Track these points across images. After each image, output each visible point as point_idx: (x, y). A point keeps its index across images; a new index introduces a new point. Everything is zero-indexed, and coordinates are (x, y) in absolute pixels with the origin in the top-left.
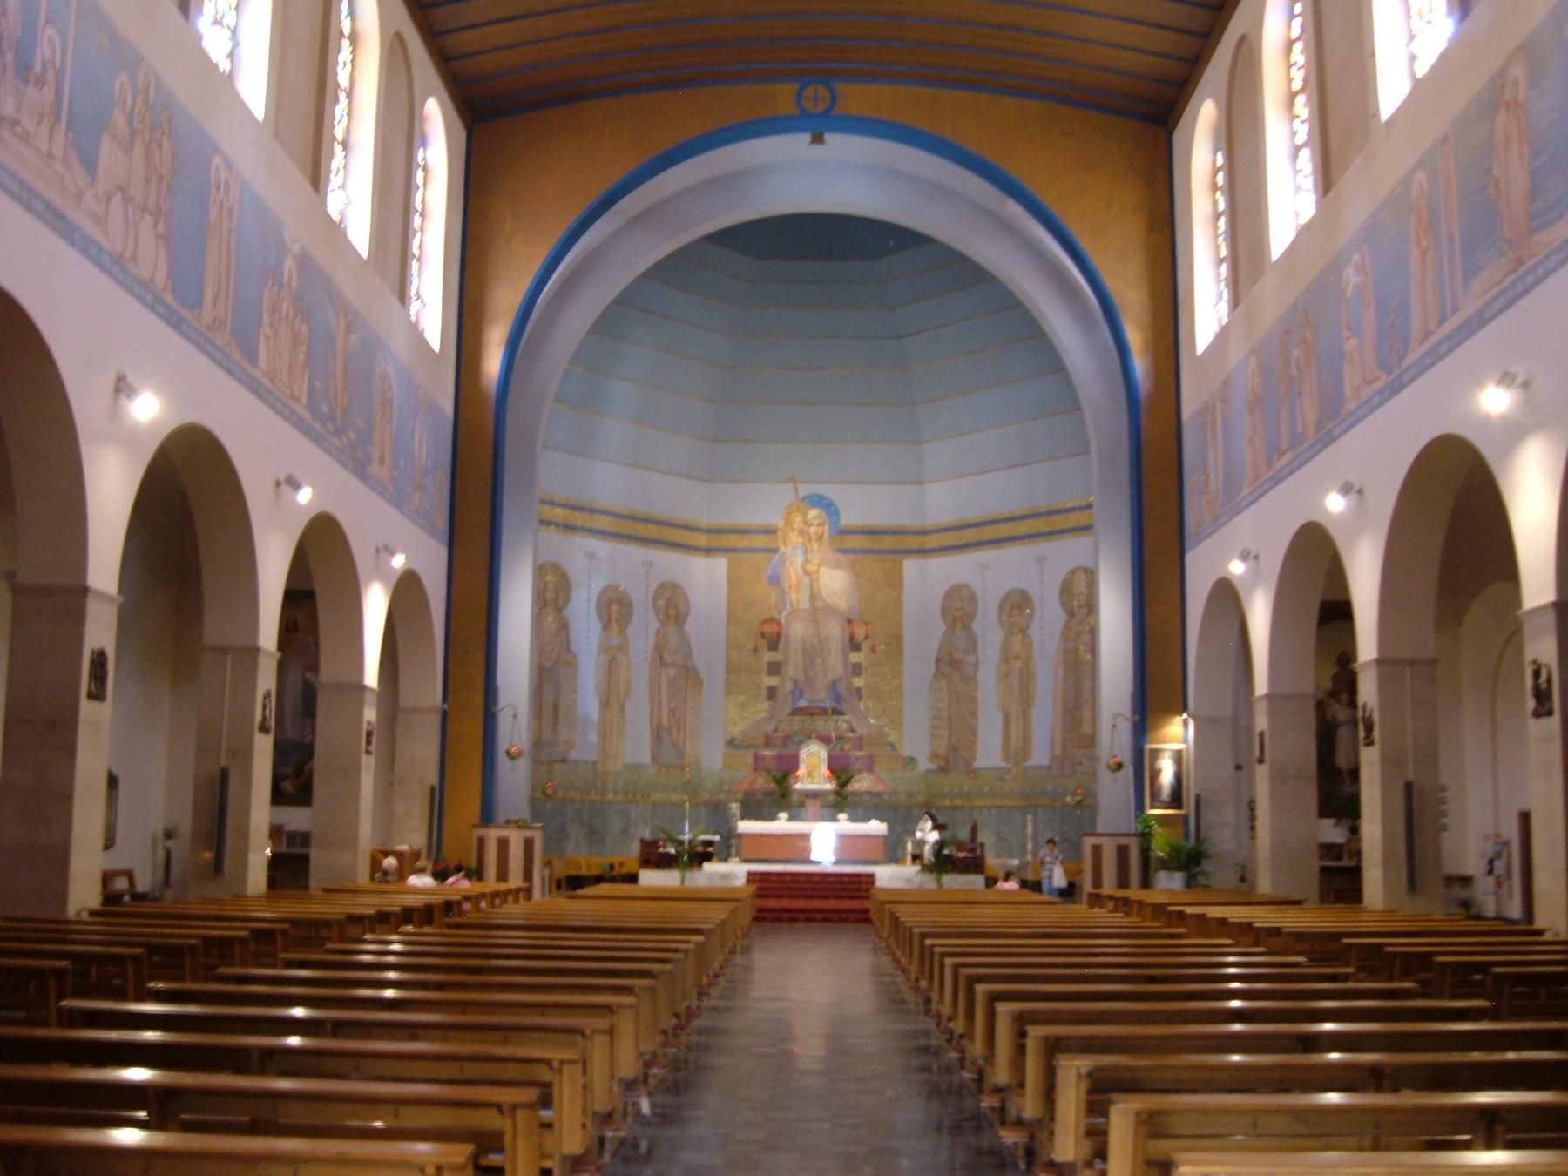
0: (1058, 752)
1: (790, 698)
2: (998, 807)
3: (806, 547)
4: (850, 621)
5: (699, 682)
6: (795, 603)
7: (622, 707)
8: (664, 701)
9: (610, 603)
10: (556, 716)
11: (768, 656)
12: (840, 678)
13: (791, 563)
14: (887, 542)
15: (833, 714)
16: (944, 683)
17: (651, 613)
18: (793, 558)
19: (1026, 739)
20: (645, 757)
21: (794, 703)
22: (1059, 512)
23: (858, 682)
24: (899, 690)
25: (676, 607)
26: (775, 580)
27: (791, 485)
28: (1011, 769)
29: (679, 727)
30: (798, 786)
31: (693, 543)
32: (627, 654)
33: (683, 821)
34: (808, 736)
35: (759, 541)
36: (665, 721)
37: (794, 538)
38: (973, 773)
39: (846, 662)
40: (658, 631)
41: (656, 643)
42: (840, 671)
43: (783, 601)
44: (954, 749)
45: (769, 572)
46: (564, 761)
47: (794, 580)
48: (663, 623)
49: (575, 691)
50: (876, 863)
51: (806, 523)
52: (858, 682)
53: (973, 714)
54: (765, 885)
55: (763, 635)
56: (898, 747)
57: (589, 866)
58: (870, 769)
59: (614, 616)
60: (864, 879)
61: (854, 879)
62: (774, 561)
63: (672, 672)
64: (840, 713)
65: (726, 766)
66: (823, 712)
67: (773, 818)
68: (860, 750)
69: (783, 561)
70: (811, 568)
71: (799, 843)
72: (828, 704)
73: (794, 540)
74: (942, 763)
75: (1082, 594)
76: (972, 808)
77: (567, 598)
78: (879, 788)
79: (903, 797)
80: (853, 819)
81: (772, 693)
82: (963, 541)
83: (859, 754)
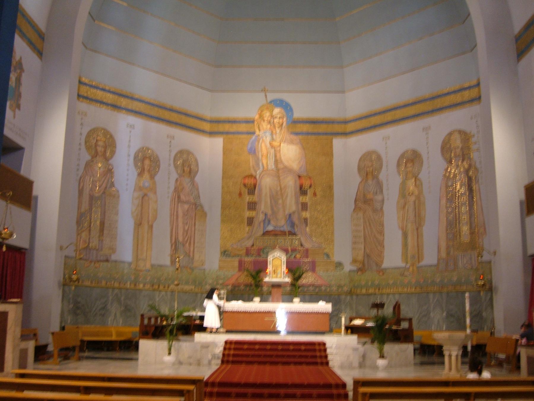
0: (444, 255)
1: (262, 224)
2: (400, 294)
3: (272, 132)
4: (299, 177)
5: (204, 215)
6: (265, 165)
7: (151, 227)
8: (180, 224)
9: (143, 161)
10: (102, 230)
11: (247, 198)
12: (294, 212)
13: (263, 140)
14: (322, 128)
15: (289, 235)
16: (361, 215)
17: (172, 168)
18: (264, 138)
19: (419, 247)
20: (167, 261)
21: (264, 227)
22: (439, 96)
23: (306, 214)
24: (331, 219)
25: (189, 166)
26: (253, 151)
27: (263, 94)
28: (409, 268)
29: (190, 243)
30: (267, 279)
31: (202, 128)
32: (155, 193)
33: (174, 301)
34: (273, 248)
35: (243, 127)
36: (181, 239)
37: (265, 125)
38: (382, 271)
39: (297, 203)
40: (177, 180)
41: (175, 188)
42: (294, 208)
43: (258, 164)
44: (367, 256)
45: (249, 146)
46: (107, 261)
47: (264, 151)
48: (180, 176)
49: (117, 214)
50: (323, 333)
51: (272, 116)
52: (306, 214)
53: (382, 233)
54: (237, 352)
55: (245, 185)
56: (331, 255)
57: (119, 334)
58: (313, 270)
59: (146, 167)
60: (317, 347)
61: (309, 347)
62: (251, 140)
63: (186, 207)
64: (294, 234)
65: (220, 268)
66: (283, 233)
67: (250, 299)
68: (307, 257)
69: (258, 139)
70: (276, 144)
71: (266, 319)
72: (287, 228)
73: (265, 127)
74: (361, 266)
75: (458, 147)
76: (382, 294)
77: (113, 153)
78: (319, 282)
79: (334, 288)
80: (303, 300)
81: (250, 221)
82: (372, 124)
83: (306, 260)
